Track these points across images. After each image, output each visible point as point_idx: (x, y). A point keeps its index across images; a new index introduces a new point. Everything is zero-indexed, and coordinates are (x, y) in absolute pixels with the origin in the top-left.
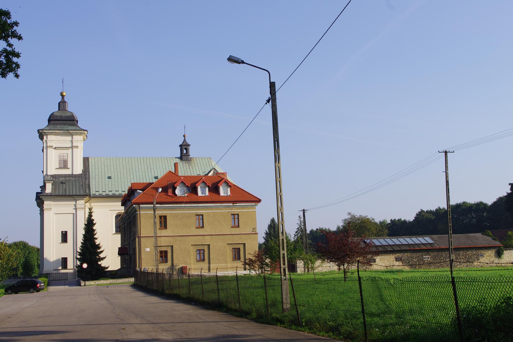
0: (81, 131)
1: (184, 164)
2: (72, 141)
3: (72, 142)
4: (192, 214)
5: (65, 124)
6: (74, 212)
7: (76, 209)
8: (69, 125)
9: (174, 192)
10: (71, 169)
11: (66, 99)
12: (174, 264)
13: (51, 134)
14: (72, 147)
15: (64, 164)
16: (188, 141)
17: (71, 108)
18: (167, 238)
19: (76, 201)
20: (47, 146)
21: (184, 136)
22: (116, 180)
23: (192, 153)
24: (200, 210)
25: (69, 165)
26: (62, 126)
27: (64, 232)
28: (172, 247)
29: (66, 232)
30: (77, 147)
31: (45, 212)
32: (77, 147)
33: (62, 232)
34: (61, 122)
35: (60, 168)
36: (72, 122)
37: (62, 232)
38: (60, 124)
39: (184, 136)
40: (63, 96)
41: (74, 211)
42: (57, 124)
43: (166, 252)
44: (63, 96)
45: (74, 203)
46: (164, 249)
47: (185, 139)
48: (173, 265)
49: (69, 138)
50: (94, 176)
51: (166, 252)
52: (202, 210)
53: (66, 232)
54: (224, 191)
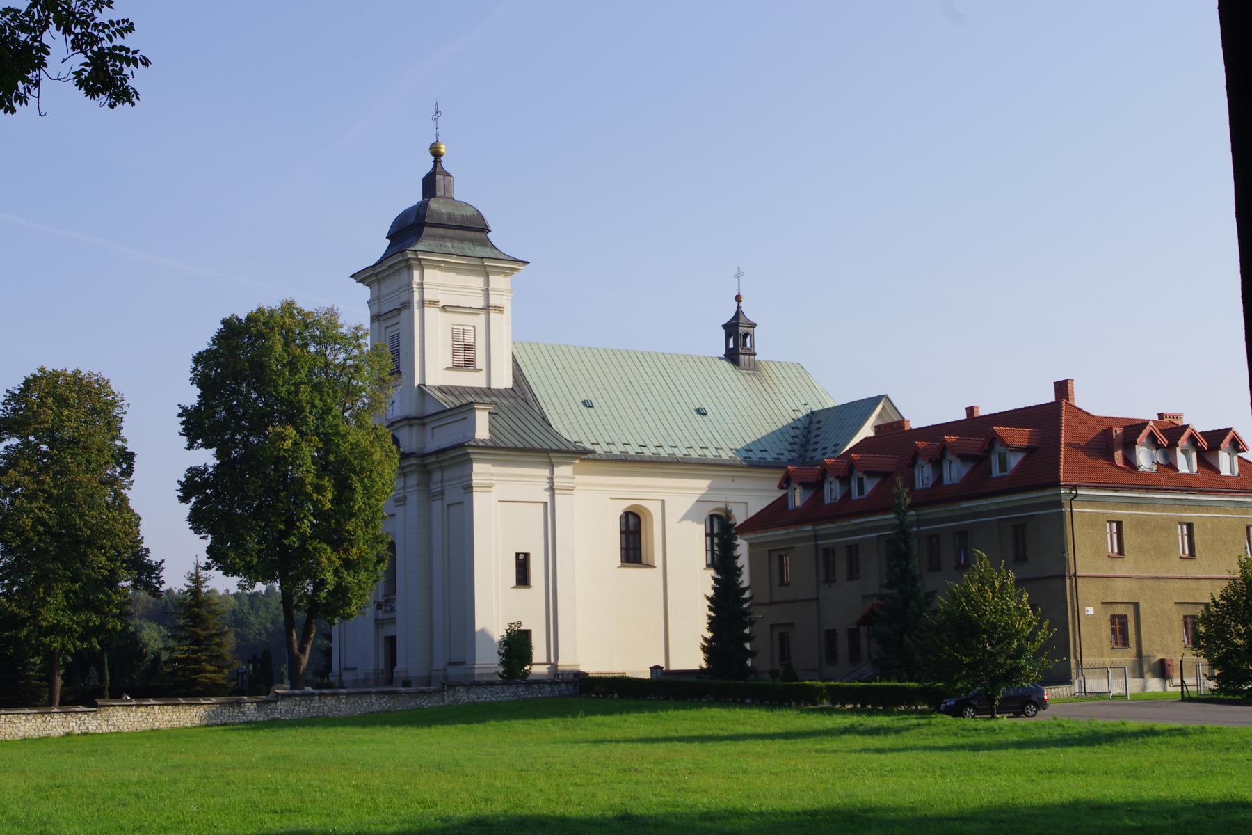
0: (511, 264)
1: (748, 377)
2: (487, 290)
3: (487, 292)
4: (1170, 519)
5: (462, 240)
6: (548, 499)
7: (552, 490)
8: (472, 241)
9: (1130, 463)
10: (484, 373)
11: (446, 163)
12: (1144, 653)
13: (435, 265)
14: (487, 308)
15: (465, 358)
16: (749, 313)
17: (468, 190)
18: (1128, 583)
19: (552, 466)
20: (423, 302)
21: (738, 299)
22: (716, 411)
23: (764, 346)
24: (1185, 511)
25: (480, 362)
26: (456, 244)
27: (521, 557)
28: (1136, 605)
29: (527, 555)
30: (499, 309)
31: (475, 494)
32: (499, 309)
33: (518, 555)
34: (451, 232)
35: (455, 367)
36: (478, 235)
37: (518, 555)
38: (452, 239)
39: (738, 299)
40: (436, 153)
41: (546, 497)
42: (442, 237)
43: (1123, 619)
44: (436, 153)
45: (546, 472)
46: (1120, 610)
47: (739, 307)
48: (1139, 654)
49: (478, 281)
50: (545, 396)
51: (1123, 619)
52: (1190, 511)
53: (527, 555)
54: (1226, 464)
